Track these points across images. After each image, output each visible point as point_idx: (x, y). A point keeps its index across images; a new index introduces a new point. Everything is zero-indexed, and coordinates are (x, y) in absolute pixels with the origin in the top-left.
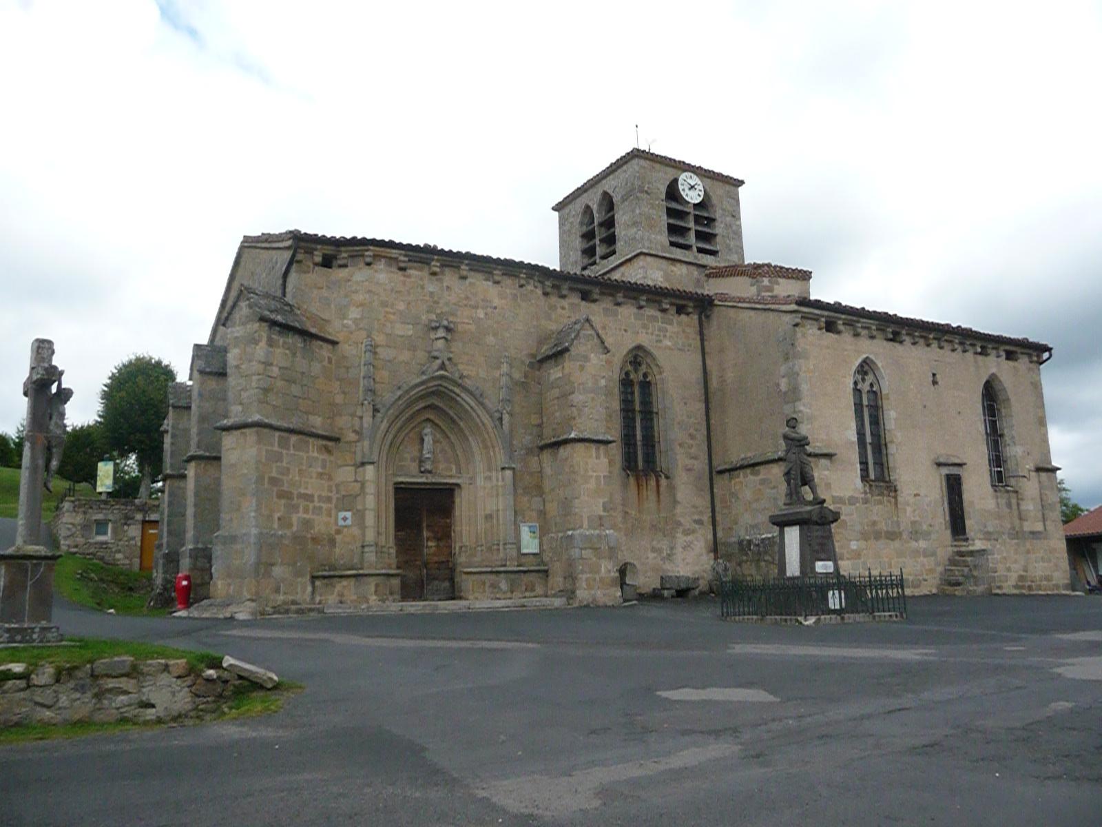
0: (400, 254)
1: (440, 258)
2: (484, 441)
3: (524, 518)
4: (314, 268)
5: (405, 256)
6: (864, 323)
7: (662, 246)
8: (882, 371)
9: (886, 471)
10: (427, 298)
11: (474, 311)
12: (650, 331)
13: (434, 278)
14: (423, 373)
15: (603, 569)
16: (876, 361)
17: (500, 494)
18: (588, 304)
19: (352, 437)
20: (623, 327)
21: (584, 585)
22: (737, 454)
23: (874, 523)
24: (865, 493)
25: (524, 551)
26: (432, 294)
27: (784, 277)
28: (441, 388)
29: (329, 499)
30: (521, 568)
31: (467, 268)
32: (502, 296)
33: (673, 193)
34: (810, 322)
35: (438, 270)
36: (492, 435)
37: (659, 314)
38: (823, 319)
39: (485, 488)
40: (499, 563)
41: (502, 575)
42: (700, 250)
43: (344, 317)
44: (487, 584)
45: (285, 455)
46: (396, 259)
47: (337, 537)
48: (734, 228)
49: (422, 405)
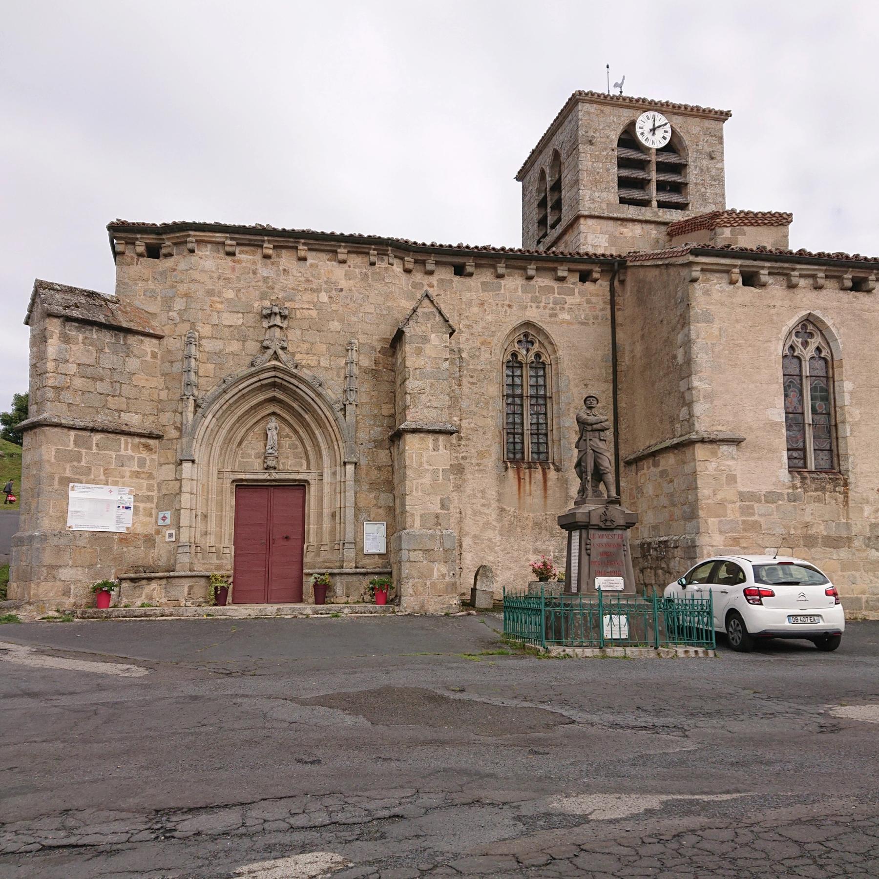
0: (226, 238)
1: (270, 238)
3: (369, 515)
4: (138, 260)
5: (231, 239)
6: (800, 269)
7: (609, 205)
8: (833, 329)
9: (835, 459)
10: (260, 284)
11: (315, 294)
12: (542, 304)
13: (268, 261)
14: (252, 365)
15: (435, 574)
16: (824, 319)
18: (462, 279)
19: (174, 434)
20: (507, 302)
21: (410, 591)
22: (644, 443)
23: (807, 526)
24: (794, 487)
26: (265, 279)
27: (752, 225)
28: (277, 380)
29: (149, 499)
30: (358, 570)
31: (306, 248)
32: (348, 276)
33: (628, 139)
34: (718, 275)
35: (270, 252)
37: (555, 285)
38: (737, 270)
41: (338, 577)
42: (662, 205)
43: (170, 309)
45: (84, 454)
46: (223, 244)
48: (714, 172)
49: (261, 397)
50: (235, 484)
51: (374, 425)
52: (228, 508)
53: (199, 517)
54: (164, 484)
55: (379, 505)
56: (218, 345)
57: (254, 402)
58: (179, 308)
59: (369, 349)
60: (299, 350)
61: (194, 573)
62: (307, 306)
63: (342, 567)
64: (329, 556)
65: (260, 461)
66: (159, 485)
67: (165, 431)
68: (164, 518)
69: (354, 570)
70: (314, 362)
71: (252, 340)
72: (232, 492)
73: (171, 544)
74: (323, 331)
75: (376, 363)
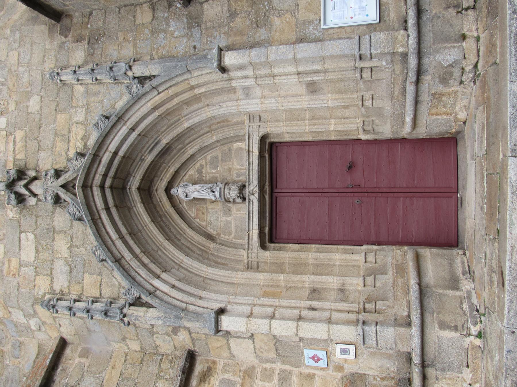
2: (187, 103)
3: (310, 22)
17: (268, 71)
19: (183, 337)
25: (373, 16)
30: (411, 21)
36: (171, 92)
39: (263, 97)
40: (398, 68)
44: (441, 88)
47: (347, 371)
49: (139, 208)
50: (268, 244)
51: (165, 31)
52: (302, 255)
53: (315, 304)
54: (261, 355)
55: (293, 8)
56: (60, 267)
57: (146, 218)
58: (22, 317)
59: (63, 52)
60: (63, 153)
61: (415, 318)
62: (11, 144)
63: (405, 55)
64: (382, 89)
65: (234, 208)
66: (263, 360)
67: (182, 347)
68: (315, 358)
69: (412, 32)
70: (79, 129)
71: (52, 219)
72: (280, 249)
73: (359, 352)
74: (40, 120)
75: (79, 40)
